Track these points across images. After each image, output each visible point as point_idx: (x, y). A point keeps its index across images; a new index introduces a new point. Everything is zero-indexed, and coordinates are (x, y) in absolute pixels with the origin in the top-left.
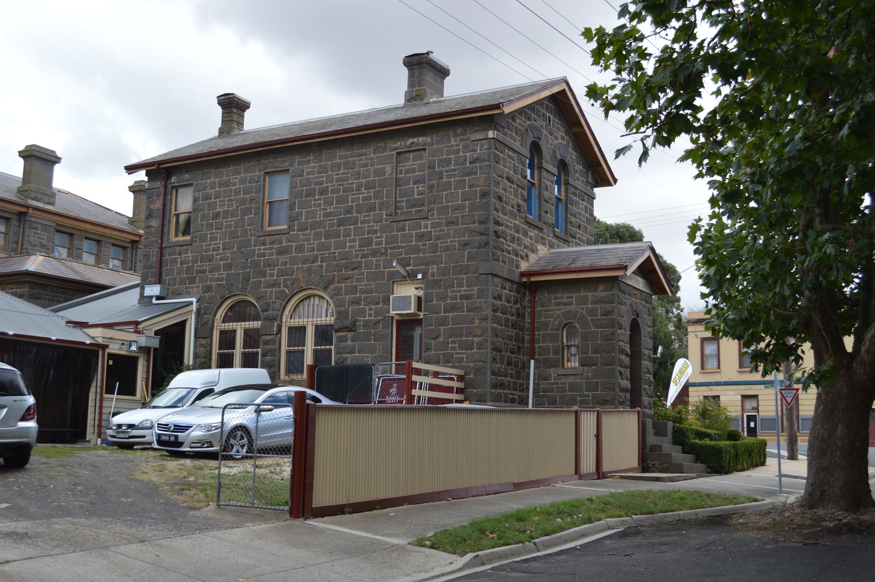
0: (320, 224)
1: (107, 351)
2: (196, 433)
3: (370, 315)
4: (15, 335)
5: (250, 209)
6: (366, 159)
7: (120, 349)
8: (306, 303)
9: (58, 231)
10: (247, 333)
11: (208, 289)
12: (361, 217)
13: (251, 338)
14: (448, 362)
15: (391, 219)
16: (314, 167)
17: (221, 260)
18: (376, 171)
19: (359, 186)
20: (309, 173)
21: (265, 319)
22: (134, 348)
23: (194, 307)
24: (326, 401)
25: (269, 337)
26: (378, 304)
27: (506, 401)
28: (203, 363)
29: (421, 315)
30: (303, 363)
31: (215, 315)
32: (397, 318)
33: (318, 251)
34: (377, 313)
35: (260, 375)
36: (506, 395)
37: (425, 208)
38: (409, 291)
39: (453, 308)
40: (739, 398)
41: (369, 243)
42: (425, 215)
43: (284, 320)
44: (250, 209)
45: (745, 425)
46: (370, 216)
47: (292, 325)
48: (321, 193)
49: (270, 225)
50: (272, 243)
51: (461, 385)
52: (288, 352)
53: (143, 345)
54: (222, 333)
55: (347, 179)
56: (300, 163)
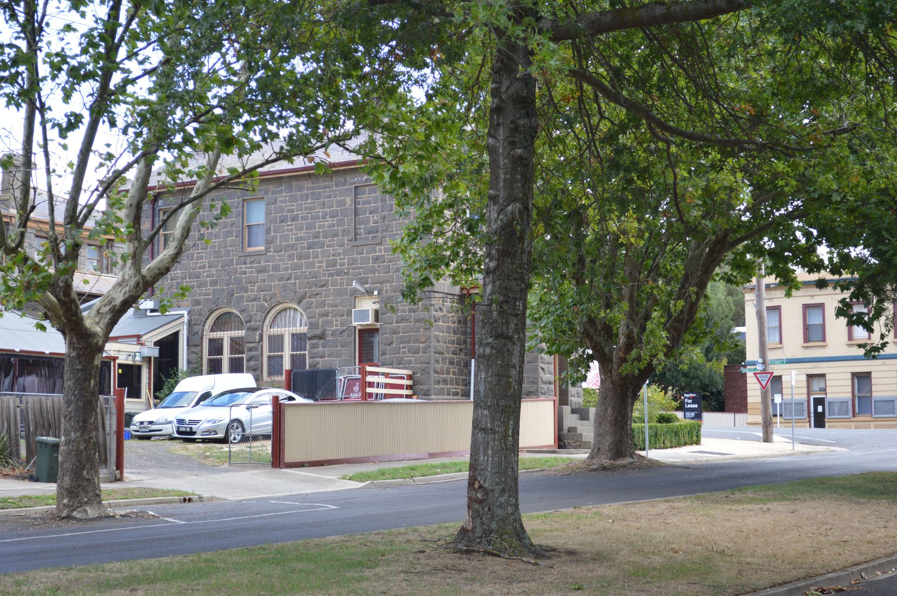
0: (292, 247)
1: (118, 361)
2: (205, 426)
3: (337, 326)
4: (51, 353)
5: (231, 232)
6: (330, 191)
7: (127, 360)
8: (283, 313)
9: (37, 236)
10: (233, 340)
11: (197, 303)
12: (327, 241)
13: (236, 344)
14: (400, 364)
15: (352, 243)
16: (286, 197)
17: (207, 277)
18: (338, 202)
19: (325, 214)
20: (282, 202)
21: (249, 329)
22: (138, 358)
23: (186, 318)
24: (299, 400)
25: (252, 345)
26: (342, 316)
27: (449, 394)
28: (195, 370)
29: (378, 325)
30: (282, 366)
31: (204, 326)
32: (359, 327)
33: (292, 270)
34: (342, 325)
35: (246, 379)
36: (449, 390)
37: (379, 235)
38: (368, 305)
39: (403, 320)
40: (804, 378)
41: (334, 265)
42: (379, 241)
43: (265, 330)
44: (231, 232)
45: (812, 410)
46: (334, 240)
47: (272, 333)
48: (293, 220)
49: (249, 245)
50: (252, 263)
51: (409, 382)
52: (269, 357)
53: (146, 355)
54: (211, 341)
55: (314, 208)
56: (274, 192)
